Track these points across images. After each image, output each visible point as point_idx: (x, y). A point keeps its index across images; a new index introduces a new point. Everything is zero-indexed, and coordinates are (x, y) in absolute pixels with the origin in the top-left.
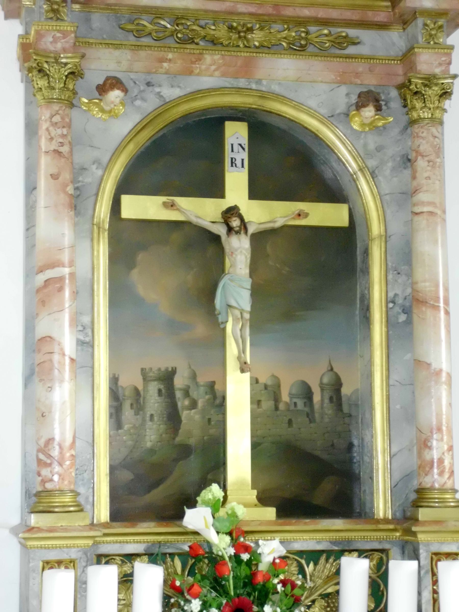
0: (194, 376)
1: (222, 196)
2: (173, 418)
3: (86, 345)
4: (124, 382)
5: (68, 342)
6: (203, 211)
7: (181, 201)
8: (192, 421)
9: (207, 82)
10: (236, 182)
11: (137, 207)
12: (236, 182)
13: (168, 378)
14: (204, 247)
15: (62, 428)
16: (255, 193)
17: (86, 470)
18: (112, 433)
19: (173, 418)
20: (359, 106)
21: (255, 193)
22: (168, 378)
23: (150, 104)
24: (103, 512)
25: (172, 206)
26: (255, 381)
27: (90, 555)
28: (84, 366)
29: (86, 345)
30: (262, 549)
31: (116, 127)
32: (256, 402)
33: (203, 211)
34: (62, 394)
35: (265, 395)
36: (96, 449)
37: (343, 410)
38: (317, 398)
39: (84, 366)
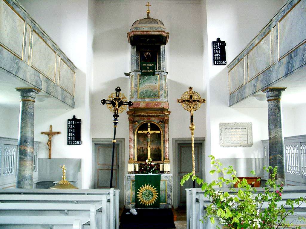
0: (145, 148)
1: (147, 130)
2: (143, 151)
3: (134, 145)
4: (139, 148)
5: (132, 145)
6: (146, 132)
7: (143, 131)
8: (145, 152)
9: (145, 120)
10: (149, 129)
11: (140, 132)
12: (149, 129)
13: (143, 148)
14: (145, 136)
15: (132, 153)
16: (151, 130)
17: (134, 157)
18: (279, 133)
19: (143, 151)
20: (160, 122)
21: (151, 130)
22: (143, 148)
23: (140, 123)
24: (136, 160)
25: (142, 132)
26: (151, 148)
27: (142, 121)
28: (134, 147)
29: (134, 145)
30: (199, 196)
31: (137, 125)
32: (151, 150)
33: (146, 132)
34: (132, 150)
35: (152, 149)
36: (86, 221)
37: (160, 150)
38: (157, 150)
39: (134, 147)
